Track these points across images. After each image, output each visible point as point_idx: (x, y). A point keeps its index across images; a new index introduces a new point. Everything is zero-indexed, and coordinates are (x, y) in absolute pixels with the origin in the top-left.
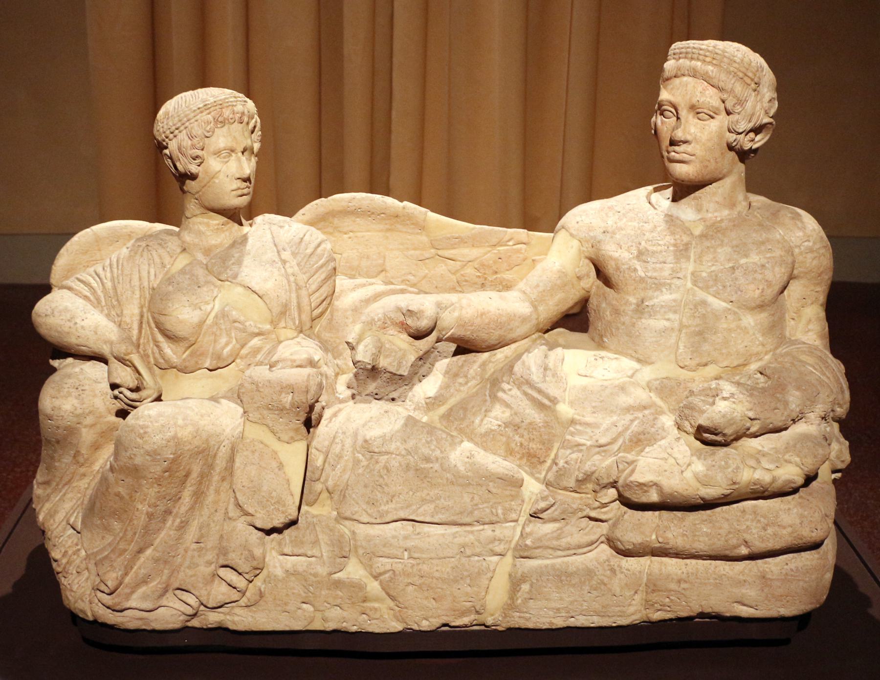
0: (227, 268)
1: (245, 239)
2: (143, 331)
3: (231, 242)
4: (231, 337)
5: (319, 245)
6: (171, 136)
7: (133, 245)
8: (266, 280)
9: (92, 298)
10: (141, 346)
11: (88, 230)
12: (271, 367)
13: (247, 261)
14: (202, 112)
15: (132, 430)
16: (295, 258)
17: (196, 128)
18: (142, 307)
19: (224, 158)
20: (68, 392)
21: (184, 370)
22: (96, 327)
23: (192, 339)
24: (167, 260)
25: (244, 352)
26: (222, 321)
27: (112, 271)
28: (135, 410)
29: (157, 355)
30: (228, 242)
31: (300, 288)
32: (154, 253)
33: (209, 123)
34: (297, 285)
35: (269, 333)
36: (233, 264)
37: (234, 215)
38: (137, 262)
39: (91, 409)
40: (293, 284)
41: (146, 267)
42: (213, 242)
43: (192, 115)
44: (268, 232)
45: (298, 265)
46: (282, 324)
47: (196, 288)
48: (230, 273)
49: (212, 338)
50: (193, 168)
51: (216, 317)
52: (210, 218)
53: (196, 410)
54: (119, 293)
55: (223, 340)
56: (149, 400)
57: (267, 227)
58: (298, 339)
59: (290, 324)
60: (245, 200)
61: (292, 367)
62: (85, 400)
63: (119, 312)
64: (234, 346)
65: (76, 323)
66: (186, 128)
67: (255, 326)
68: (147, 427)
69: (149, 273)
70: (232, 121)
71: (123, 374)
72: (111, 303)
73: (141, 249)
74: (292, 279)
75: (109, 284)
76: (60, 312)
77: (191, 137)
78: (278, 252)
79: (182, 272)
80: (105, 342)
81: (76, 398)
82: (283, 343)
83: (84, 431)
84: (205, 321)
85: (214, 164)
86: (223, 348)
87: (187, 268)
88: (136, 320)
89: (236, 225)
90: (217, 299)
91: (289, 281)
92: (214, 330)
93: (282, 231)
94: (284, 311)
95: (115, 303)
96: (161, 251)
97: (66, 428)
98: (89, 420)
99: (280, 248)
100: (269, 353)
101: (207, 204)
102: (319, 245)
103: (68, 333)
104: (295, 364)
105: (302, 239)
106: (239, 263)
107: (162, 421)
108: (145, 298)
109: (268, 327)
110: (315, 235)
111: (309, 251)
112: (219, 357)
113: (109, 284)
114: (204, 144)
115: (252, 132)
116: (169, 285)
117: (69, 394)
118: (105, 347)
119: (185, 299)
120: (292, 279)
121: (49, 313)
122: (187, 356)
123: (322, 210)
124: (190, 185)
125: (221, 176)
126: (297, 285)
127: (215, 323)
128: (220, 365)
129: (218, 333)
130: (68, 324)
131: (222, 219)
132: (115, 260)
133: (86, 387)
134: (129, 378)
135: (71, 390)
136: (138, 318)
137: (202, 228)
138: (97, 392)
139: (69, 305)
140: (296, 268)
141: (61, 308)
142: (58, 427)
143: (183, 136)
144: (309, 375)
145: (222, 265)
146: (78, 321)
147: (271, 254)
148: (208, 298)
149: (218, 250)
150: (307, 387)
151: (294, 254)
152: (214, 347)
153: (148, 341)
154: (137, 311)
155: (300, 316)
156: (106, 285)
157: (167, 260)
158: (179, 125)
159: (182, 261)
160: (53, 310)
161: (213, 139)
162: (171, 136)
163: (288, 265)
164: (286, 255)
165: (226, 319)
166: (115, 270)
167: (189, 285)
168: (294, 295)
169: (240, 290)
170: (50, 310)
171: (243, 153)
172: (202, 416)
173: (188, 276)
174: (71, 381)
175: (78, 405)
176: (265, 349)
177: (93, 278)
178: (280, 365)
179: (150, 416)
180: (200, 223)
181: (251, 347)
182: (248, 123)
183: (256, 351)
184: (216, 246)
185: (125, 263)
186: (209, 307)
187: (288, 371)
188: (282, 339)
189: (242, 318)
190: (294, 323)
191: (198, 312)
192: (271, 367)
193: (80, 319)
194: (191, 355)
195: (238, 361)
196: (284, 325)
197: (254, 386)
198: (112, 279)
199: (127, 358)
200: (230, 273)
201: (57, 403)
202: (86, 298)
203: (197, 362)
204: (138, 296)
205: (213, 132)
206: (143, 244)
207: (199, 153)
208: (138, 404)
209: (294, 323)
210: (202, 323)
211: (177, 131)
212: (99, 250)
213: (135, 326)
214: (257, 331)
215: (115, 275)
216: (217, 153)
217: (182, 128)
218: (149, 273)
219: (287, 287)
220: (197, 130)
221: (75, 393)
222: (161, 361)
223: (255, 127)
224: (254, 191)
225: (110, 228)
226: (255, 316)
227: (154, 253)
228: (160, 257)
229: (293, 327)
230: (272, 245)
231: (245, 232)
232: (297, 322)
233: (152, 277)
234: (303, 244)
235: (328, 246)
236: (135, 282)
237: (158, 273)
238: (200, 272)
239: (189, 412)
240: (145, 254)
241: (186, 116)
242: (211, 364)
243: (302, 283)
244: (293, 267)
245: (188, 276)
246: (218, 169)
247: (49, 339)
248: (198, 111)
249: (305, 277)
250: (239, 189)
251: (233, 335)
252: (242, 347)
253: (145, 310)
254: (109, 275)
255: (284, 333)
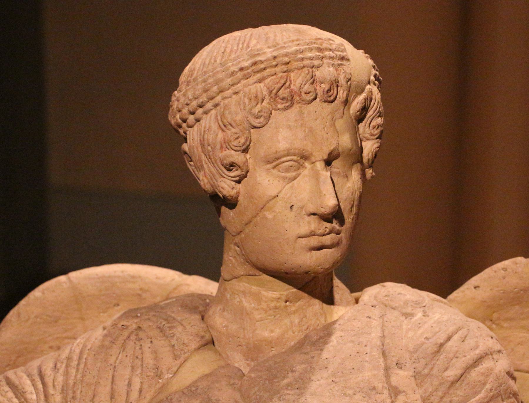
0: (277, 392)
1: (327, 332)
3: (300, 336)
5: (477, 362)
6: (191, 118)
7: (114, 325)
11: (62, 278)
14: (247, 77)
17: (233, 109)
19: (287, 170)
24: (167, 361)
27: (66, 374)
30: (294, 337)
32: (146, 345)
33: (258, 99)
37: (316, 286)
38: (112, 360)
41: (127, 372)
42: (266, 334)
43: (229, 81)
50: (226, 187)
52: (262, 285)
57: (376, 312)
66: (216, 106)
69: (130, 384)
70: (309, 97)
73: (126, 333)
77: (224, 127)
78: (387, 369)
85: (265, 182)
87: (203, 385)
93: (406, 324)
96: (161, 343)
101: (254, 259)
102: (477, 362)
105: (441, 345)
110: (481, 337)
111: (452, 373)
114: (249, 140)
115: (360, 119)
123: (513, 281)
124: (228, 216)
125: (279, 206)
131: (286, 290)
132: (78, 351)
137: (247, 304)
143: (209, 121)
149: (274, 352)
151: (419, 377)
157: (167, 361)
158: (204, 98)
161: (266, 132)
162: (191, 118)
164: (401, 377)
166: (73, 372)
171: (328, 163)
177: (32, 381)
180: (244, 293)
182: (346, 102)
184: (270, 343)
185: (90, 361)
205: (268, 119)
206: (133, 324)
207: (238, 158)
211: (200, 111)
212: (82, 319)
215: (71, 382)
216: (274, 161)
217: (209, 105)
218: (130, 384)
220: (236, 112)
223: (364, 110)
225: (102, 279)
230: (377, 354)
231: (335, 317)
235: (501, 364)
237: (145, 386)
240: (130, 344)
241: (218, 82)
246: (273, 193)
248: (240, 75)
250: (312, 234)
254: (60, 379)
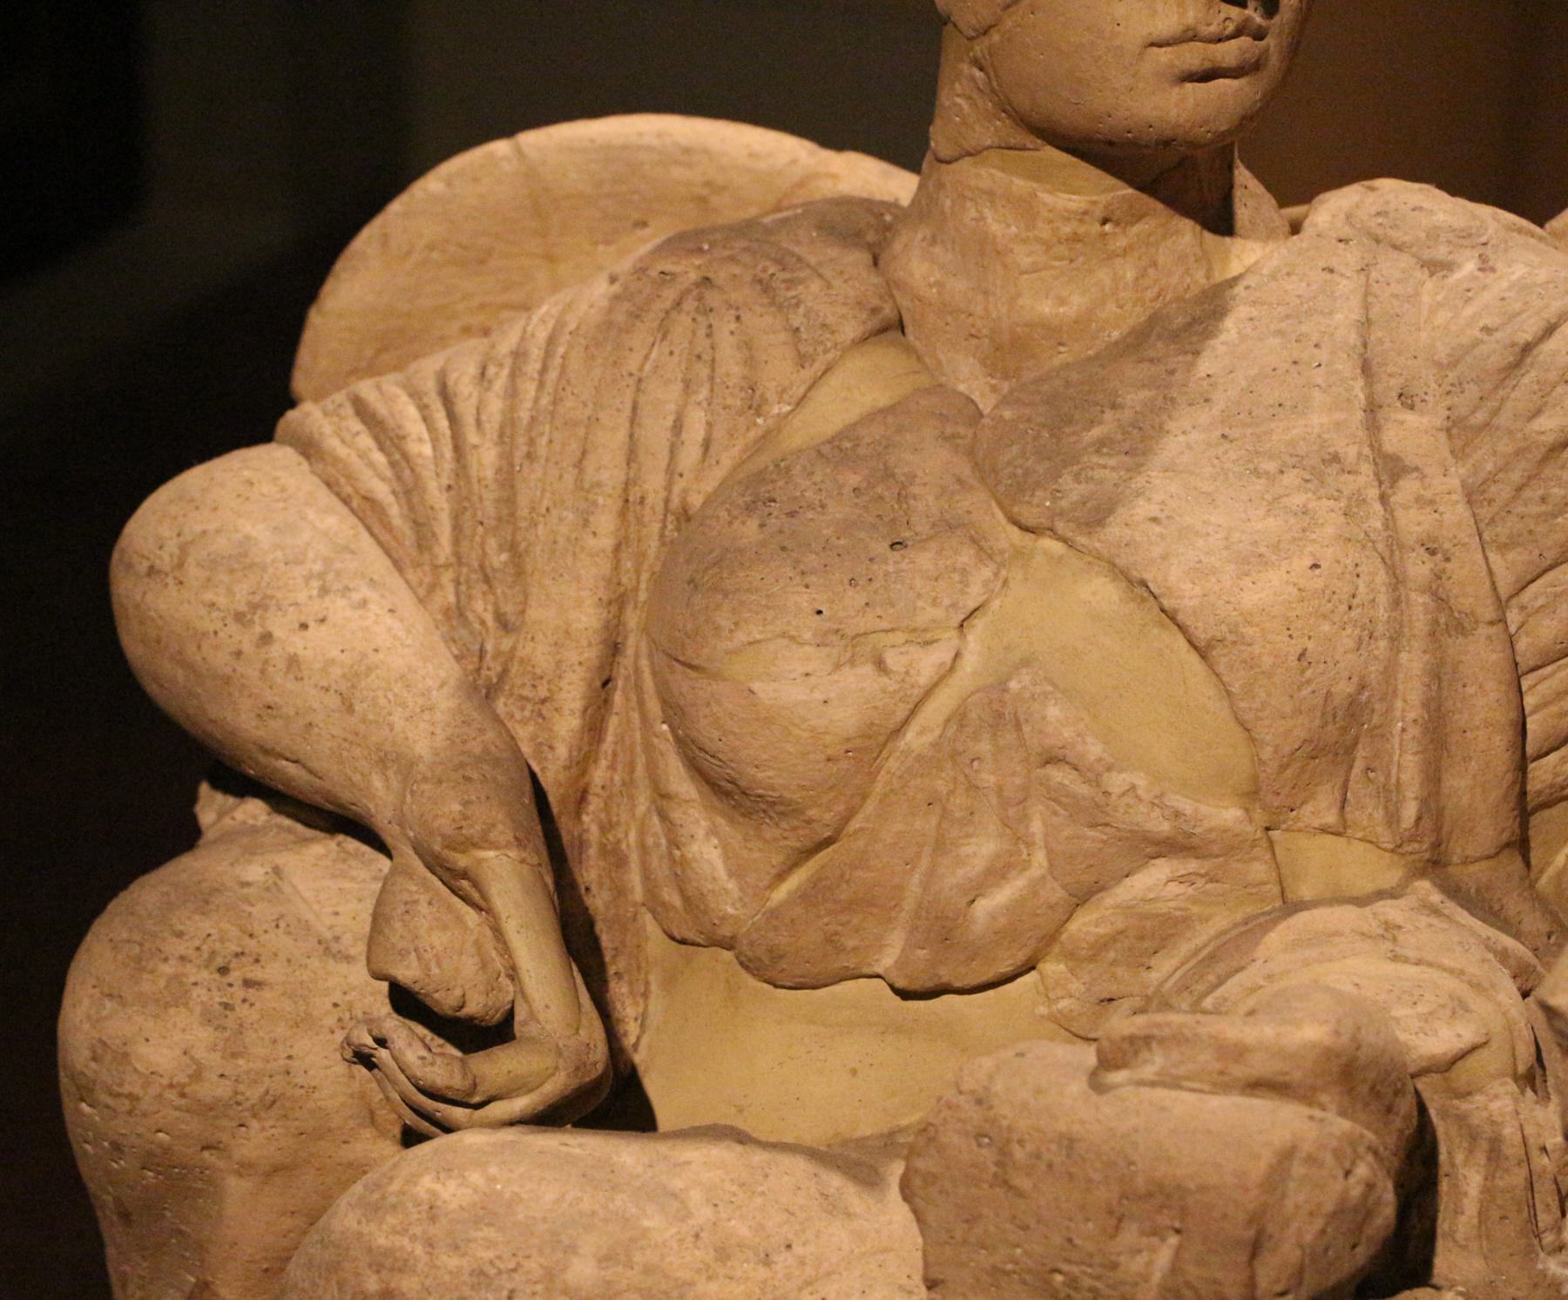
1: (1211, 306)
2: (613, 723)
3: (1136, 316)
4: (1021, 839)
7: (640, 271)
8: (1252, 561)
9: (395, 512)
10: (594, 804)
11: (500, 147)
12: (1107, 1062)
13: (1186, 436)
15: (335, 1267)
16: (1459, 454)
18: (618, 602)
20: (176, 978)
21: (770, 969)
22: (354, 677)
23: (824, 817)
24: (779, 370)
25: (1085, 925)
26: (984, 747)
27: (512, 393)
28: (443, 1140)
29: (661, 870)
30: (1119, 319)
31: (1460, 627)
34: (1441, 601)
35: (1229, 851)
36: (1100, 445)
38: (633, 363)
39: (277, 1085)
40: (1419, 600)
42: (1046, 308)
44: (1347, 285)
45: (1472, 496)
46: (1321, 808)
47: (882, 547)
48: (1073, 490)
49: (927, 824)
51: (959, 717)
53: (704, 1214)
54: (523, 501)
55: (982, 848)
56: (519, 1105)
57: (1350, 258)
58: (1391, 910)
59: (1367, 814)
60: (1225, 99)
61: (1222, 1085)
62: (250, 1037)
63: (509, 609)
64: (1034, 889)
65: (267, 638)
67: (1157, 802)
68: (404, 1266)
69: (678, 427)
71: (438, 940)
72: (468, 554)
73: (670, 294)
74: (1418, 568)
75: (486, 458)
76: (213, 564)
78: (1372, 409)
79: (839, 449)
80: (383, 762)
81: (208, 1019)
82: (1302, 918)
83: (236, 1187)
84: (898, 731)
86: (976, 890)
87: (876, 431)
88: (581, 657)
89: (1187, 232)
90: (979, 623)
91: (1397, 580)
92: (941, 786)
94: (1338, 739)
95: (499, 559)
96: (762, 321)
97: (155, 1159)
98: (258, 1141)
99: (1388, 386)
100: (1212, 958)
101: (1022, 101)
103: (227, 680)
104: (1239, 1071)
105: (1527, 349)
106: (1137, 443)
107: (485, 1247)
108: (641, 556)
109: (1229, 815)
112: (942, 929)
113: (486, 458)
116: (749, 509)
117: (178, 995)
118: (377, 782)
119: (803, 600)
120: (1418, 568)
121: (165, 560)
122: (788, 902)
126: (1441, 601)
127: (948, 753)
128: (945, 975)
129: (959, 802)
130: (236, 636)
131: (1094, 190)
132: (542, 335)
133: (271, 972)
134: (469, 965)
135: (194, 974)
136: (592, 654)
137: (998, 226)
138: (321, 1004)
139: (261, 534)
140: (1456, 513)
141: (221, 545)
142: (117, 1147)
144: (1287, 1155)
145: (1055, 435)
146: (279, 626)
147: (1328, 419)
148: (928, 614)
149: (1065, 356)
150: (1256, 1219)
152: (931, 873)
153: (629, 783)
154: (588, 619)
155: (1433, 777)
156: (472, 460)
157: (779, 370)
159: (857, 390)
160: (184, 549)
163: (1408, 487)
164: (1411, 432)
165: (1009, 737)
166: (529, 389)
167: (846, 528)
168: (1413, 662)
169: (1102, 592)
170: (172, 546)
172: (723, 1254)
173: (853, 480)
174: (206, 925)
175: (214, 1060)
176: (1203, 935)
177: (423, 409)
178: (1154, 1063)
179: (433, 1212)
181: (1126, 909)
183: (1153, 933)
184: (1055, 333)
185: (575, 364)
186: (927, 663)
187: (1182, 1103)
188: (1306, 892)
189: (1094, 750)
190: (1392, 818)
191: (860, 681)
192: (1107, 1062)
193: (293, 617)
194: (805, 897)
195: (1052, 967)
196: (1331, 818)
197: (988, 1155)
198: (505, 435)
199: (462, 861)
200: (1073, 490)
201: (120, 1025)
202: (366, 510)
203: (831, 939)
204: (607, 542)
206: (688, 270)
208: (458, 1113)
209: (1392, 818)
210: (875, 741)
212: (550, 258)
213: (572, 695)
214: (1164, 828)
215: (524, 415)
218: (678, 427)
219: (1382, 613)
221: (204, 987)
222: (672, 896)
224: (1294, 50)
225: (622, 157)
226: (1162, 745)
227: (725, 326)
228: (749, 352)
229: (1386, 839)
230: (1346, 367)
232: (1410, 811)
233: (690, 455)
234: (1529, 379)
236: (607, 470)
237: (719, 434)
238: (929, 462)
239: (653, 1221)
240: (682, 322)
242: (901, 964)
243: (1472, 598)
244: (1436, 502)
245: (853, 480)
247: (153, 689)
249: (1506, 567)
250: (1189, 36)
251: (1036, 827)
252: (1081, 898)
253: (633, 619)
255: (1318, 859)
